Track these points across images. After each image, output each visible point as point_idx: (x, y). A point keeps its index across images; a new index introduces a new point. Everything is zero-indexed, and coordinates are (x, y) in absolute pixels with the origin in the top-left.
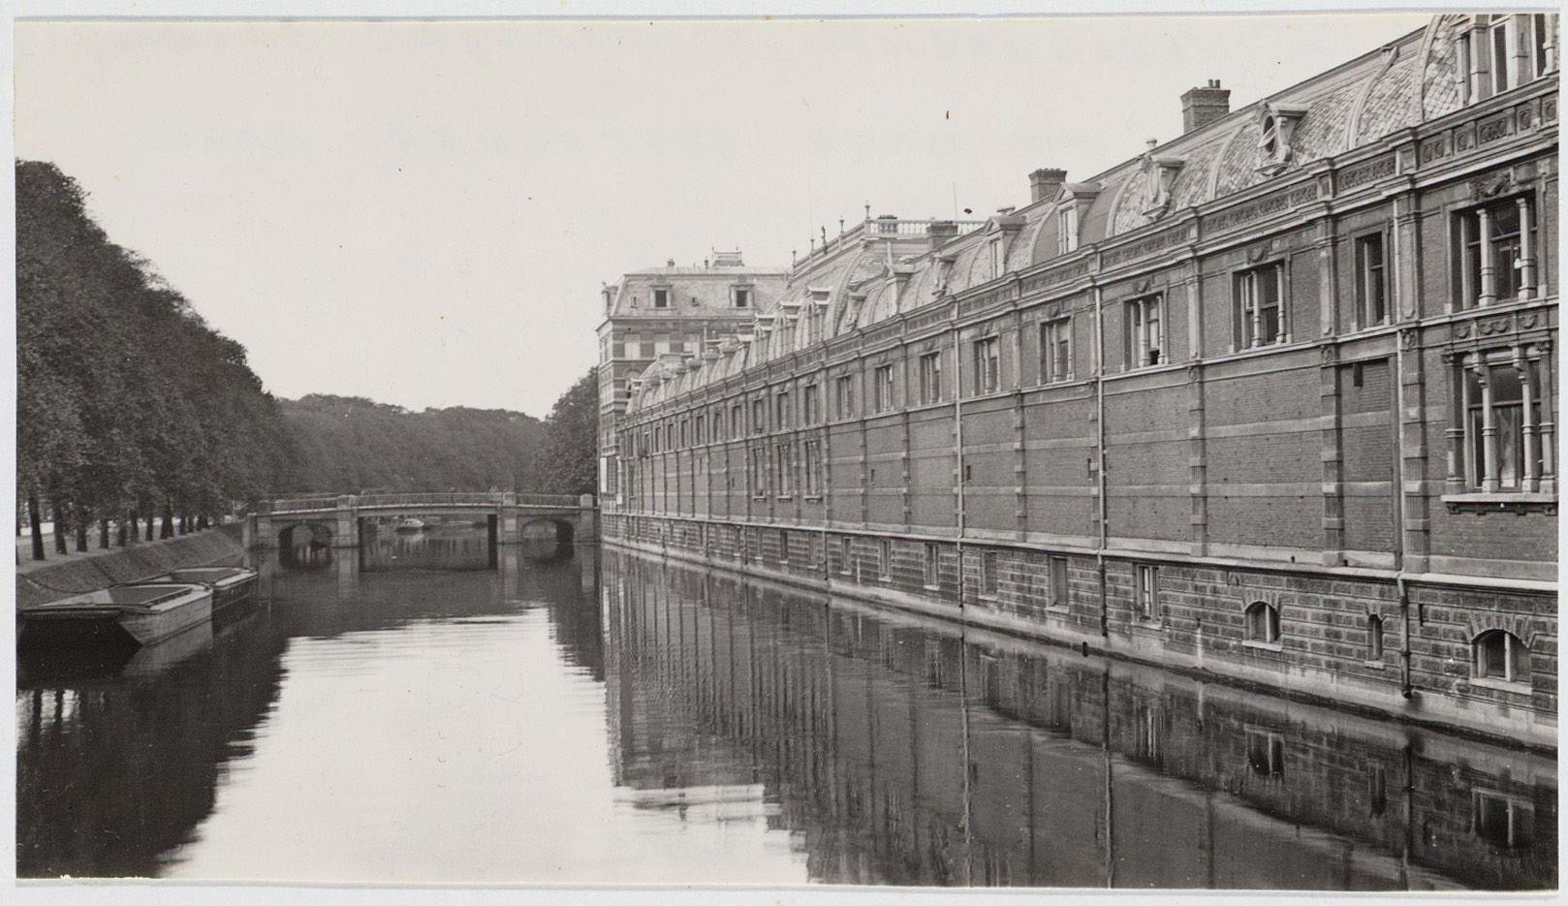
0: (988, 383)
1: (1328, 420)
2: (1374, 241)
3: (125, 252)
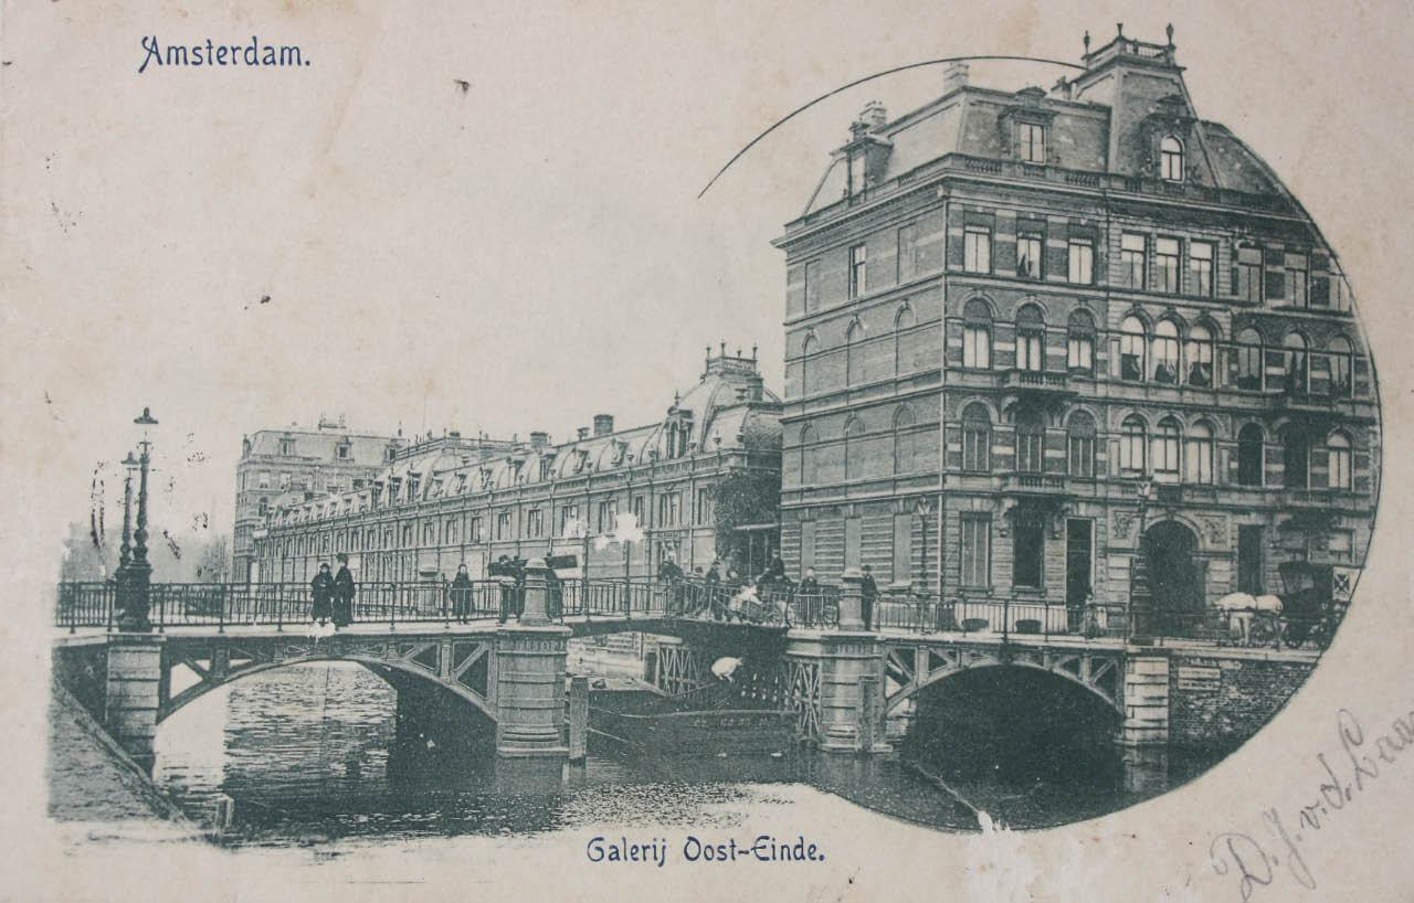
0: (607, 525)
1: (624, 562)
2: (640, 499)
3: (156, 816)
